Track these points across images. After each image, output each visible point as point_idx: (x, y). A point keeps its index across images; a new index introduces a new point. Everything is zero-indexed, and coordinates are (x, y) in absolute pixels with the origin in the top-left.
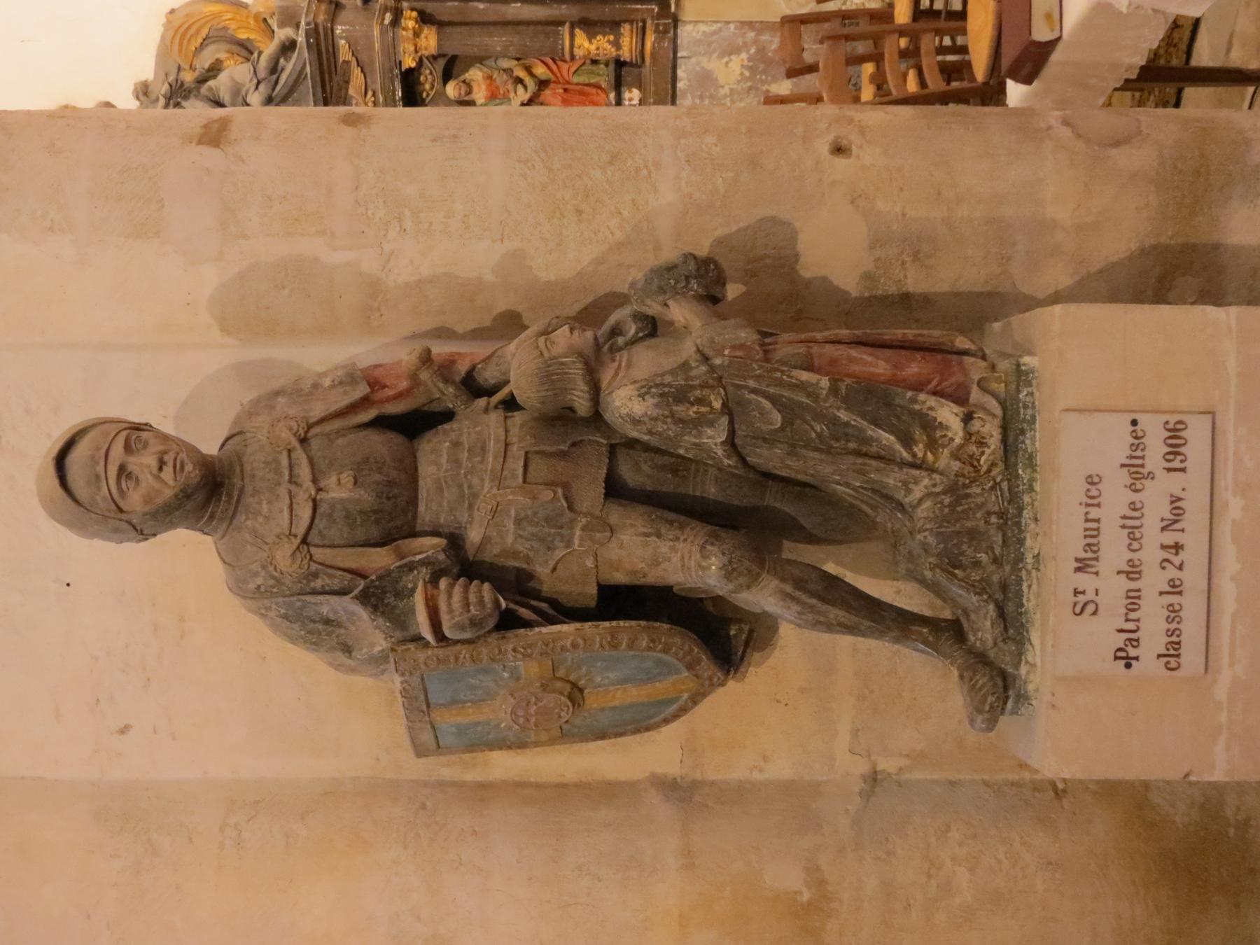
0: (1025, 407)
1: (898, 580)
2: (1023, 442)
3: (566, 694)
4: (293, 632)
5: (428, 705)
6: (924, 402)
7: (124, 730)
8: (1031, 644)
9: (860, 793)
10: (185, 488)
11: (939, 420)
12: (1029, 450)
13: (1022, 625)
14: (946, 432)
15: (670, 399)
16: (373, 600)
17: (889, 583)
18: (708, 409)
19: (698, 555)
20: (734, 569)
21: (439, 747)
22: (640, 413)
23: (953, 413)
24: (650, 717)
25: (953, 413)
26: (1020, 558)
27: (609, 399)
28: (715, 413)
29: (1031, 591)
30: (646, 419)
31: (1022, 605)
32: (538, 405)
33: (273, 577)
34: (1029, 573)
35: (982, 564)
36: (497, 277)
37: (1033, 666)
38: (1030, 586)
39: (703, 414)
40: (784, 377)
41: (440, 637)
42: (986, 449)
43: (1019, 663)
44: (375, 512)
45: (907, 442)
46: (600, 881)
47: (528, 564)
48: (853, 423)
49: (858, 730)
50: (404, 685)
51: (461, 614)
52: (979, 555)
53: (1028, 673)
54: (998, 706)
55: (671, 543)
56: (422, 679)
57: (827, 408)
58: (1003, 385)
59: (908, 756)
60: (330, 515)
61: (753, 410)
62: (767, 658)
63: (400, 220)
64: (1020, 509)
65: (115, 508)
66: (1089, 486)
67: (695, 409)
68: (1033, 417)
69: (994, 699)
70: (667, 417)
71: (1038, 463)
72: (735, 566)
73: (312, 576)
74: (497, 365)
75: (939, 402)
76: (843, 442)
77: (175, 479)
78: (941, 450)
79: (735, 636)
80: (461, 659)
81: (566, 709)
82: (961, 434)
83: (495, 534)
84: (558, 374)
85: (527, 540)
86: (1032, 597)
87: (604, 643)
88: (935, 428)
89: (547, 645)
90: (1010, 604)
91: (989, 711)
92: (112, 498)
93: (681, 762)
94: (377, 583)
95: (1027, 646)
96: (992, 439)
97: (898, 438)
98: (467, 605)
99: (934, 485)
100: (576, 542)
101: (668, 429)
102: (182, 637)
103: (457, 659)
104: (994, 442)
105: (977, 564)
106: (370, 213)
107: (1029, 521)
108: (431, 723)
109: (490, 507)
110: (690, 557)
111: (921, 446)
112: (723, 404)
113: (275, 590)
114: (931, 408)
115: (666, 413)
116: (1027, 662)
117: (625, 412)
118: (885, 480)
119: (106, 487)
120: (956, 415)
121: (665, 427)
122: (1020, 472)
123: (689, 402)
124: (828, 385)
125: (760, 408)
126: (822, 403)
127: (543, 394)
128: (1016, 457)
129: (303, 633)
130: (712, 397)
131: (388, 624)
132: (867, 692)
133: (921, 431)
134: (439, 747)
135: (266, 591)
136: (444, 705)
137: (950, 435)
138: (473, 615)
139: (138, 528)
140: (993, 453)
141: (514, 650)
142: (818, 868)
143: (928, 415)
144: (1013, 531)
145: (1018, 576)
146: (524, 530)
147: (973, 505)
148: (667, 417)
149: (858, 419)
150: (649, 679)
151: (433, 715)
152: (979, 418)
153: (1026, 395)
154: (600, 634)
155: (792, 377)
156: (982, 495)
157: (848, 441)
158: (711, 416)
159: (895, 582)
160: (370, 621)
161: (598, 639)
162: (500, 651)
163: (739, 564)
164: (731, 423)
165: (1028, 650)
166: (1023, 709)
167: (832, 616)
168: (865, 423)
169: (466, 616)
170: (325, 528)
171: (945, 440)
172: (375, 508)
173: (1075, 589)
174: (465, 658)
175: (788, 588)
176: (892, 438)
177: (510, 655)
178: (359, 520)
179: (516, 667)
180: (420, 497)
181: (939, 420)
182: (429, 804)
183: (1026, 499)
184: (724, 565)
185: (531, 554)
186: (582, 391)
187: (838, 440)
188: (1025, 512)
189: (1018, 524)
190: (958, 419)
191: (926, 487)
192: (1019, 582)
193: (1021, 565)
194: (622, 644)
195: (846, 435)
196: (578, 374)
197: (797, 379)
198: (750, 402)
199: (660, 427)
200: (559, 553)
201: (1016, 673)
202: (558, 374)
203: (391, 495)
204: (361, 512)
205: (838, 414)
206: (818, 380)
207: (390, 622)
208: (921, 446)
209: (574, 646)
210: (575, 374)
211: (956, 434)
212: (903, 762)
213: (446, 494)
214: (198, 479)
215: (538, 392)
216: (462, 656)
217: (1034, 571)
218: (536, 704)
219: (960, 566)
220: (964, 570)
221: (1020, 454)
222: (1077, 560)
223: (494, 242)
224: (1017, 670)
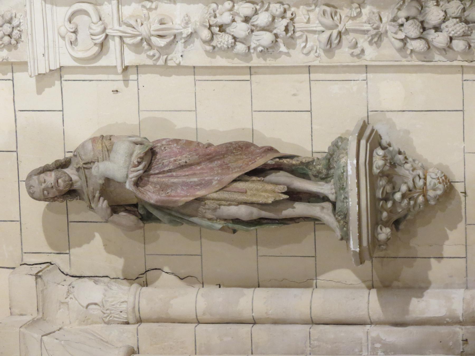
186: (354, 14)
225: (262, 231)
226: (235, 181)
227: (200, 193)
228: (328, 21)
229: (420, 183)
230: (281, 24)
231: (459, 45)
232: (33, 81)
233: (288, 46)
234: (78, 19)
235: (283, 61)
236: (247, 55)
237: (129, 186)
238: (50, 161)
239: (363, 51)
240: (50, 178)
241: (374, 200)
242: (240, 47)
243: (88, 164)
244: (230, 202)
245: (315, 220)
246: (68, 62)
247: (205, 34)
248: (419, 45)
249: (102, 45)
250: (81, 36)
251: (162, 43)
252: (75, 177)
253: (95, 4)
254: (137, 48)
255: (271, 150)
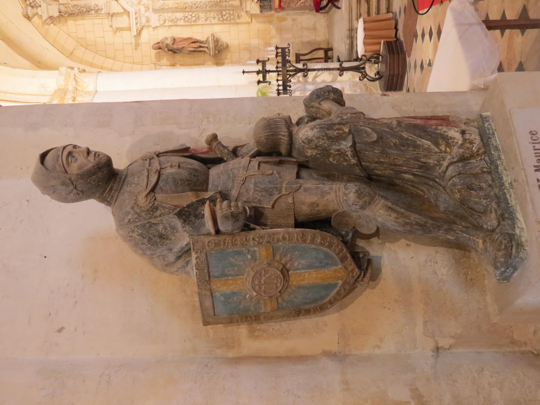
0: (489, 129)
1: (436, 246)
2: (491, 141)
3: (280, 269)
4: (145, 246)
5: (209, 277)
6: (441, 130)
7: (60, 330)
8: (518, 219)
9: (432, 356)
10: (98, 163)
11: (449, 136)
12: (495, 144)
13: (511, 212)
14: (454, 140)
15: (325, 129)
16: (184, 217)
17: (432, 248)
18: (343, 132)
19: (343, 189)
20: (362, 193)
21: (215, 315)
22: (311, 136)
23: (455, 131)
24: (323, 298)
25: (455, 131)
26: (502, 185)
27: (297, 137)
28: (346, 133)
29: (512, 197)
30: (314, 139)
31: (509, 204)
32: (265, 141)
33: (136, 213)
34: (508, 190)
35: (484, 189)
36: (247, 138)
37: (522, 228)
38: (510, 196)
39: (341, 134)
40: (376, 122)
41: (218, 232)
42: (474, 145)
43: (514, 228)
44: (188, 180)
45: (437, 145)
46: (299, 398)
47: (261, 204)
48: (410, 138)
49: (427, 322)
50: (197, 260)
51: (226, 210)
52: (481, 184)
53: (520, 232)
54: (509, 246)
55: (330, 186)
56: (207, 256)
57: (397, 132)
58: (476, 122)
59: (453, 337)
60: (167, 180)
61: (363, 133)
62: (378, 284)
63: (208, 118)
64: (497, 167)
65: (64, 170)
66: (532, 136)
67: (337, 132)
68: (493, 133)
69: (506, 242)
70: (323, 136)
71: (500, 149)
72: (362, 191)
73: (156, 209)
74: (247, 148)
75: (448, 128)
76: (406, 147)
77: (95, 160)
78: (453, 147)
79: (362, 257)
80: (226, 244)
81: (280, 280)
82: (461, 139)
83: (244, 191)
84: (274, 125)
85: (260, 192)
86: (513, 200)
87: (299, 238)
88: (449, 139)
89: (270, 237)
90: (502, 204)
91: (505, 249)
92: (64, 167)
93: (338, 343)
94: (186, 209)
95: (516, 220)
96: (476, 140)
97: (432, 143)
98: (230, 206)
99: (453, 158)
100: (284, 190)
101: (325, 143)
102: (95, 281)
103: (224, 243)
104: (478, 141)
105: (481, 189)
106: (196, 116)
107: (502, 170)
108: (211, 290)
109: (242, 179)
110: (339, 191)
111: (443, 146)
112: (349, 130)
113: (137, 220)
114: (445, 132)
115: (324, 134)
116: (518, 227)
117: (305, 137)
118: (429, 161)
119: (61, 159)
120: (457, 132)
121: (323, 142)
122: (493, 152)
123: (334, 130)
124: (396, 123)
125: (366, 132)
126: (394, 130)
127: (266, 134)
128: (489, 147)
129: (149, 246)
130: (344, 128)
131: (191, 229)
132: (429, 301)
133: (442, 140)
134: (215, 315)
135: (133, 221)
136: (217, 277)
137: (456, 141)
138: (233, 211)
139: (74, 184)
140: (478, 145)
141: (254, 239)
142: (417, 389)
143: (444, 134)
144: (496, 175)
145: (503, 192)
146: (259, 187)
147: (473, 166)
148: (323, 136)
149: (412, 136)
150: (322, 267)
151: (212, 284)
152: (468, 133)
153: (488, 125)
154: (296, 232)
155: (379, 122)
156: (477, 163)
157: (408, 147)
158: (344, 135)
159: (435, 247)
160: (182, 228)
161: (296, 235)
162: (246, 240)
163: (364, 190)
164: (353, 137)
165: (517, 222)
166: (521, 253)
167: (412, 218)
168: (415, 137)
169: (229, 211)
170: (163, 186)
171: (454, 144)
172: (188, 178)
173: (537, 179)
174: (228, 243)
175: (390, 204)
176: (429, 143)
177: (251, 243)
178: (180, 183)
179: (254, 252)
180: (210, 181)
181: (449, 136)
182: (209, 365)
183: (499, 162)
184: (357, 191)
185: (262, 199)
186: (285, 132)
187: (404, 146)
188: (499, 168)
189: (498, 172)
190: (459, 133)
191: (449, 159)
192: (505, 194)
193: (503, 188)
194: (308, 239)
195: (407, 144)
196: (283, 124)
197: (381, 122)
198: (361, 130)
199: (321, 142)
200: (275, 197)
201: (514, 233)
202: (274, 125)
203: (196, 175)
204: (181, 179)
205: (403, 134)
206: (391, 122)
207: (192, 227)
208: (443, 146)
209: (284, 238)
210: (281, 124)
211: (459, 139)
212: (452, 341)
213: (222, 177)
214: (106, 161)
215: (265, 133)
216: (227, 241)
217: (511, 189)
218: (264, 275)
219: (473, 189)
220: (476, 191)
221: (491, 146)
222: (535, 166)
223: (246, 124)
224: (514, 231)
225: (195, 54)
226: (190, 43)
227: (184, 46)
228: (205, 15)
229: (223, 44)
230: (197, 16)
231: (229, 19)
232: (152, 29)
233: (198, 20)
234: (161, 17)
235: (197, 23)
236: (191, 22)
237: (171, 45)
238: (156, 42)
239: (212, 21)
240: (156, 45)
241: (215, 46)
242: (190, 21)
243: (163, 42)
244: (189, 47)
245: (205, 51)
246: (158, 25)
247: (183, 18)
248: (221, 19)
249: (165, 21)
250: (161, 19)
251: (175, 20)
252: (161, 45)
253: (163, 14)
254: (171, 21)
255: (196, 39)
